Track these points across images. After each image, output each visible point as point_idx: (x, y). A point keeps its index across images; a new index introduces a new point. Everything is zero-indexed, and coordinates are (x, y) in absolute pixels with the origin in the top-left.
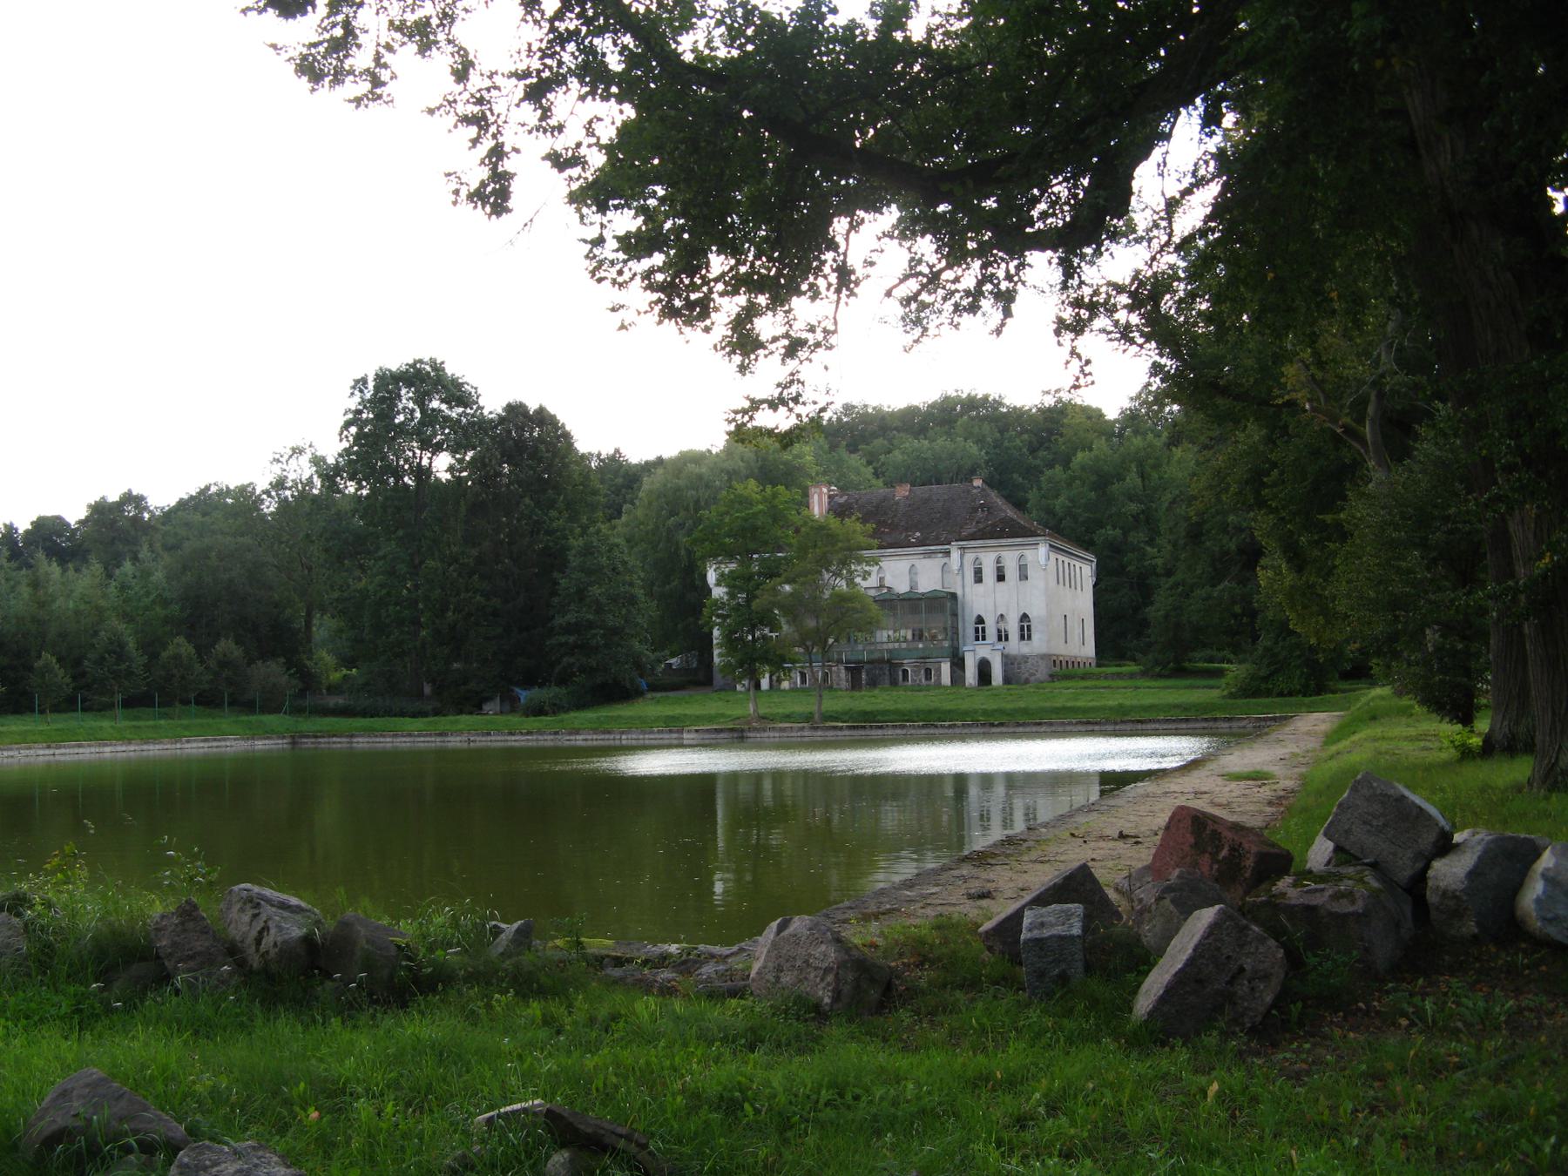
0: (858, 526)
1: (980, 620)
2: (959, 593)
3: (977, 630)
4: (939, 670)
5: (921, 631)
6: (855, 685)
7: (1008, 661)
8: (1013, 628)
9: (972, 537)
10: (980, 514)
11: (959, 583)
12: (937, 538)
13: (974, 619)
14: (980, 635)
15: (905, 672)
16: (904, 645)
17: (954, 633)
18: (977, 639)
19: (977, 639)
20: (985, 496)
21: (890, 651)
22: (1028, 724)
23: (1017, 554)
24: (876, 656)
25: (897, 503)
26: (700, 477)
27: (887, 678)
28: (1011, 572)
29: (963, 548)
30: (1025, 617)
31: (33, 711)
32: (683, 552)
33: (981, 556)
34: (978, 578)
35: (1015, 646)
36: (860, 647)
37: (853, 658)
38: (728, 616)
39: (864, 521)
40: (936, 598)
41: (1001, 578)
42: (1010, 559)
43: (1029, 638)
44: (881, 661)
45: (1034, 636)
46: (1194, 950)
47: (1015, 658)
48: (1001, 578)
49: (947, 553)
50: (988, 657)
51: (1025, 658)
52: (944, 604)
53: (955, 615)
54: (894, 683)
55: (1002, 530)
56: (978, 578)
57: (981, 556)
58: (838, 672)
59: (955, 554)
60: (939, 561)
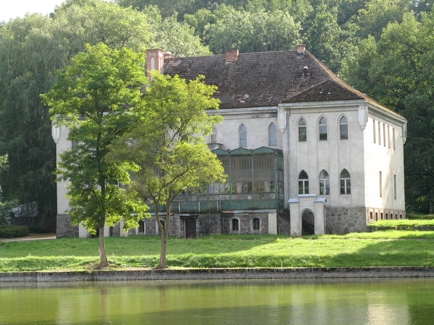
0: (203, 87)
1: (303, 175)
2: (285, 150)
3: (300, 183)
4: (266, 220)
5: (250, 184)
6: (190, 233)
7: (330, 212)
8: (334, 181)
9: (297, 99)
10: (303, 79)
11: (285, 141)
12: (265, 100)
13: (299, 171)
14: (304, 187)
15: (235, 222)
16: (234, 197)
17: (279, 185)
18: (301, 192)
19: (301, 192)
20: (309, 62)
21: (222, 202)
22: (358, 270)
23: (338, 115)
24: (210, 206)
25: (227, 68)
26: (44, 41)
27: (219, 227)
28: (333, 132)
29: (288, 109)
30: (345, 173)
31: (305, 127)
32: (27, 110)
33: (306, 117)
34: (303, 138)
35: (336, 199)
36: (194, 199)
37: (188, 208)
38: (80, 168)
39: (208, 82)
40: (264, 154)
41: (323, 137)
42: (332, 120)
43: (349, 192)
44: (213, 211)
45: (353, 191)
46: (51, 255)
47: (336, 209)
48: (323, 137)
49: (274, 114)
50: (311, 208)
51: (345, 210)
52: (271, 159)
53: (281, 170)
54: (225, 231)
55: (325, 93)
56: (303, 138)
57: (306, 117)
58: (174, 222)
59: (282, 115)
60: (267, 120)
